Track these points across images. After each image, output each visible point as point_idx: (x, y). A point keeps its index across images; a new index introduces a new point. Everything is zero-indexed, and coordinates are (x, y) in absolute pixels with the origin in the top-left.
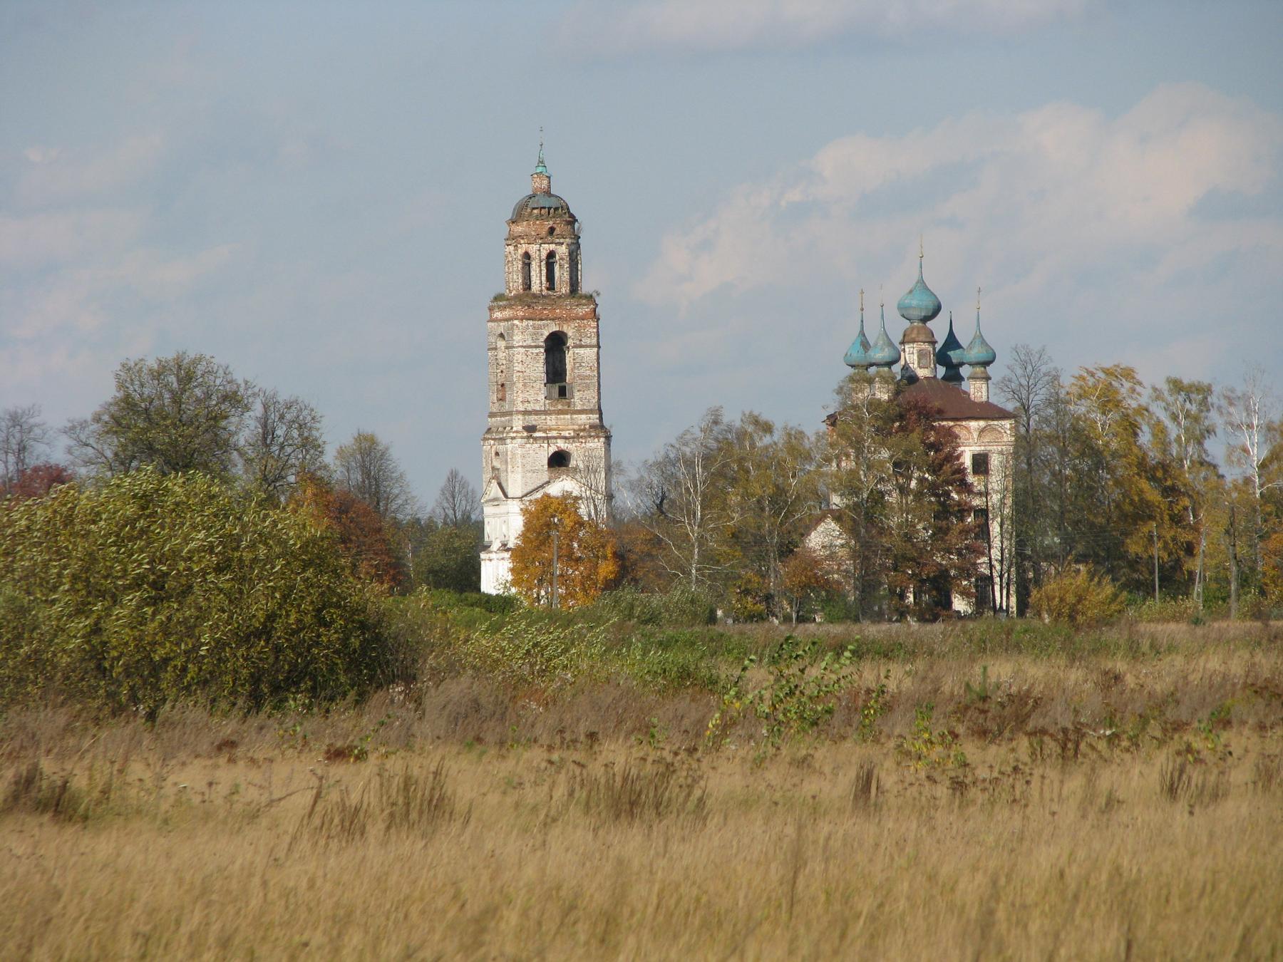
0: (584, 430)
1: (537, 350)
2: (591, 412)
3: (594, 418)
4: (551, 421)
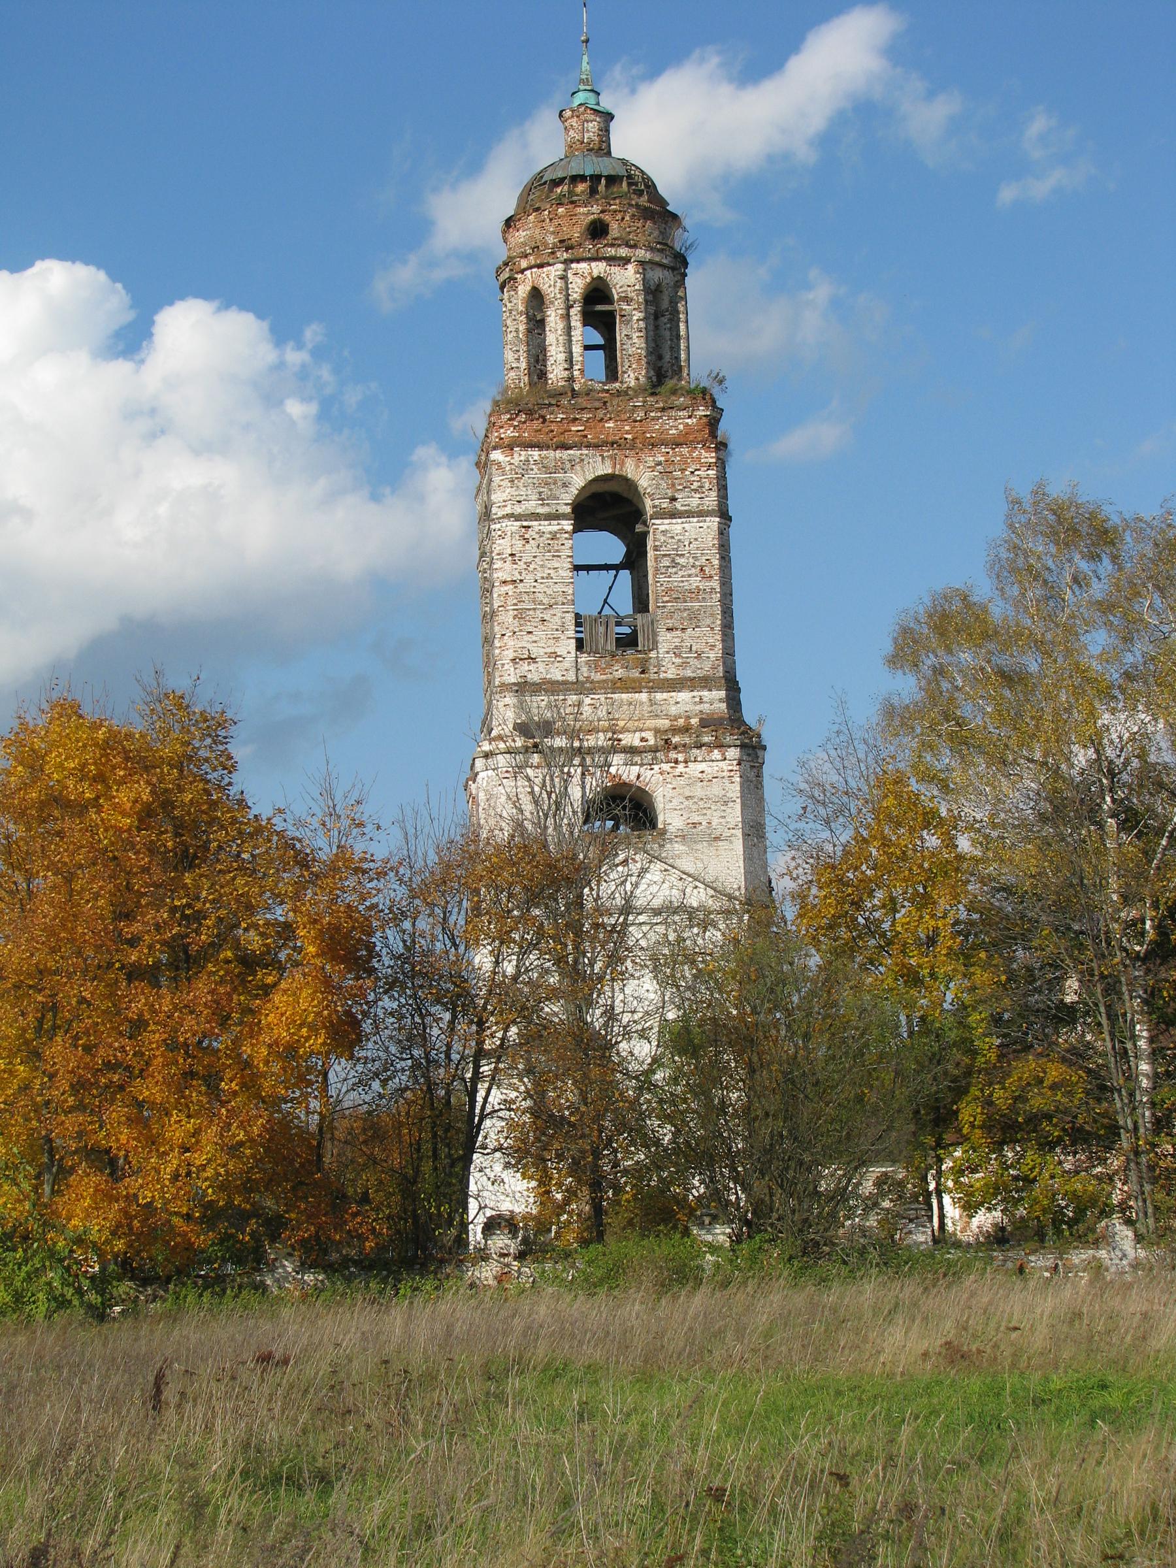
0: (686, 729)
1: (554, 527)
2: (705, 682)
3: (714, 700)
4: (592, 707)
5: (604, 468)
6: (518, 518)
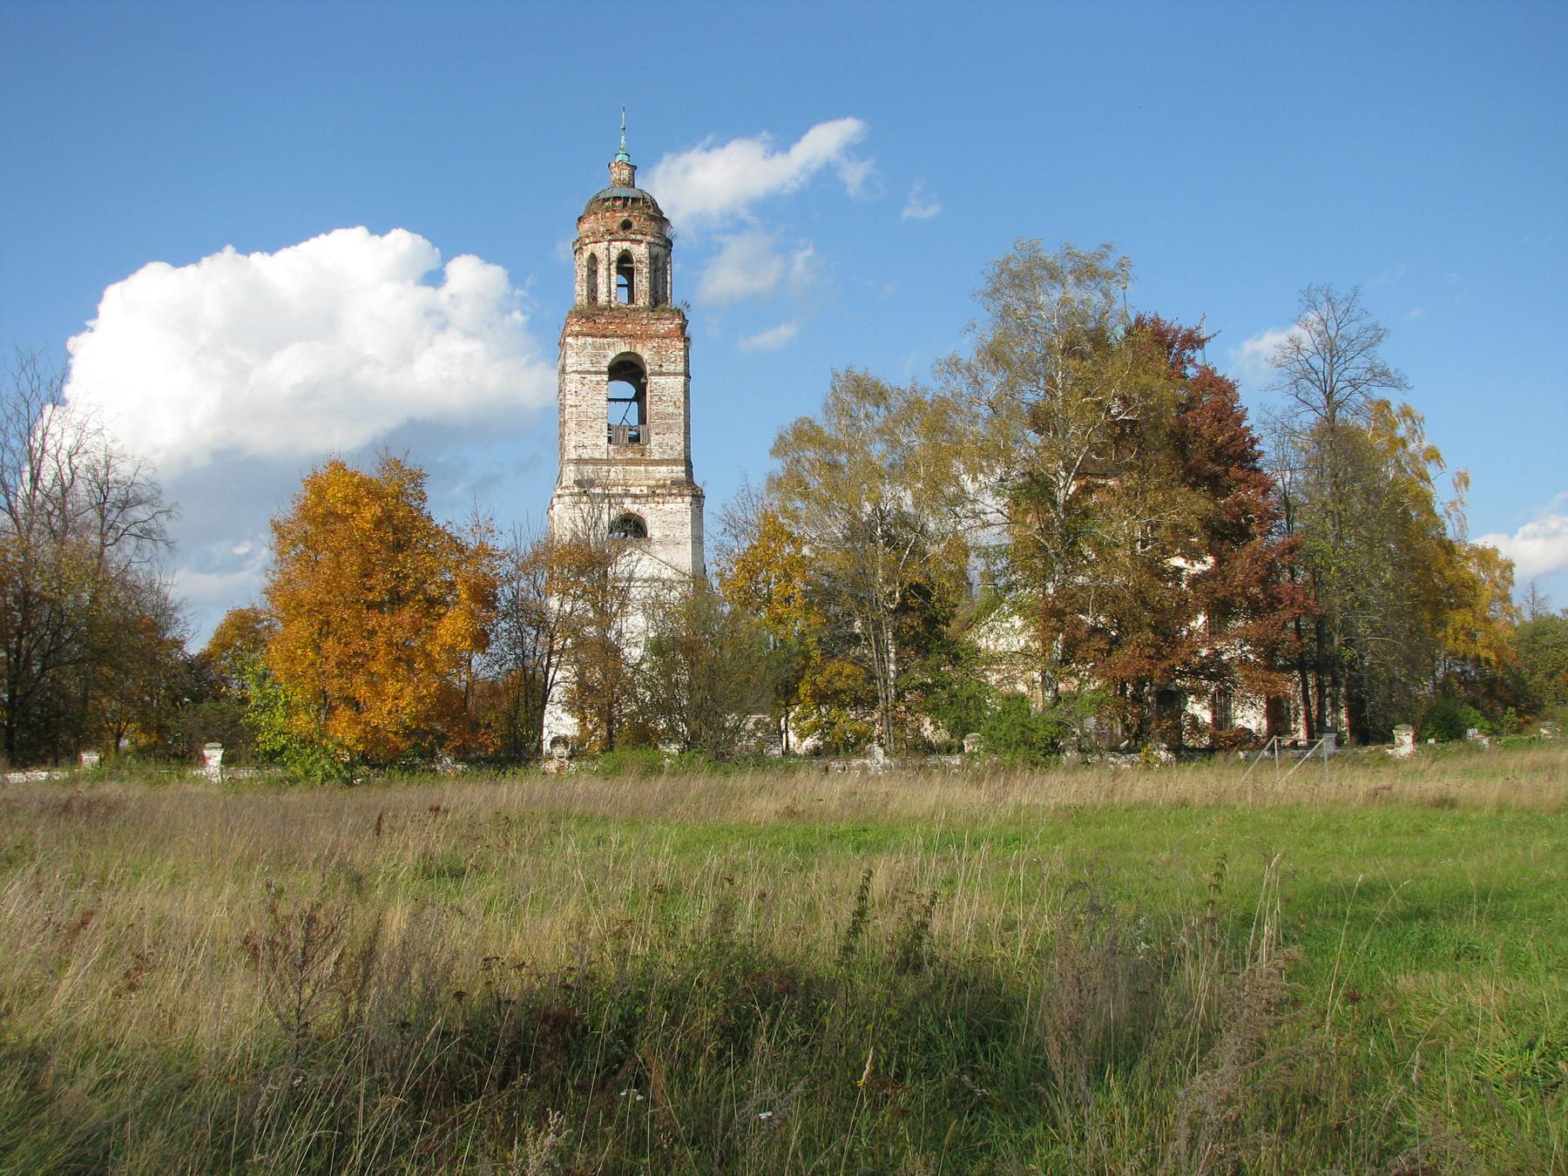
2: (674, 462)
5: (626, 349)
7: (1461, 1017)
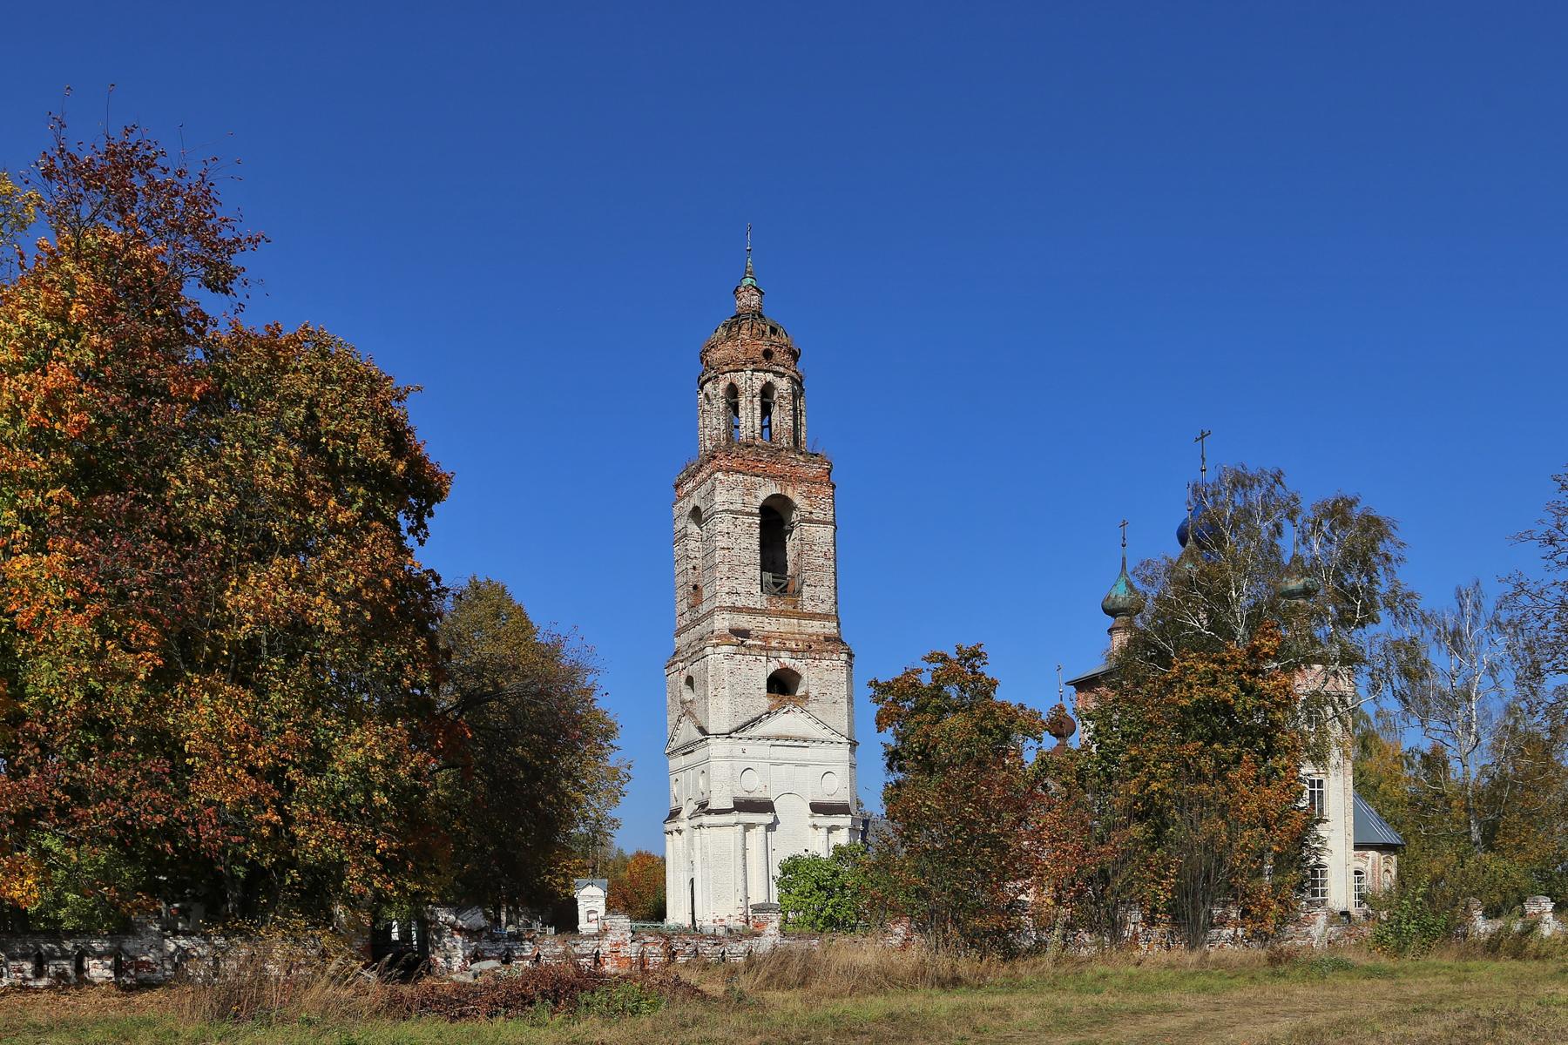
2: (825, 617)
5: (776, 491)
6: (732, 512)
7: (332, 967)
